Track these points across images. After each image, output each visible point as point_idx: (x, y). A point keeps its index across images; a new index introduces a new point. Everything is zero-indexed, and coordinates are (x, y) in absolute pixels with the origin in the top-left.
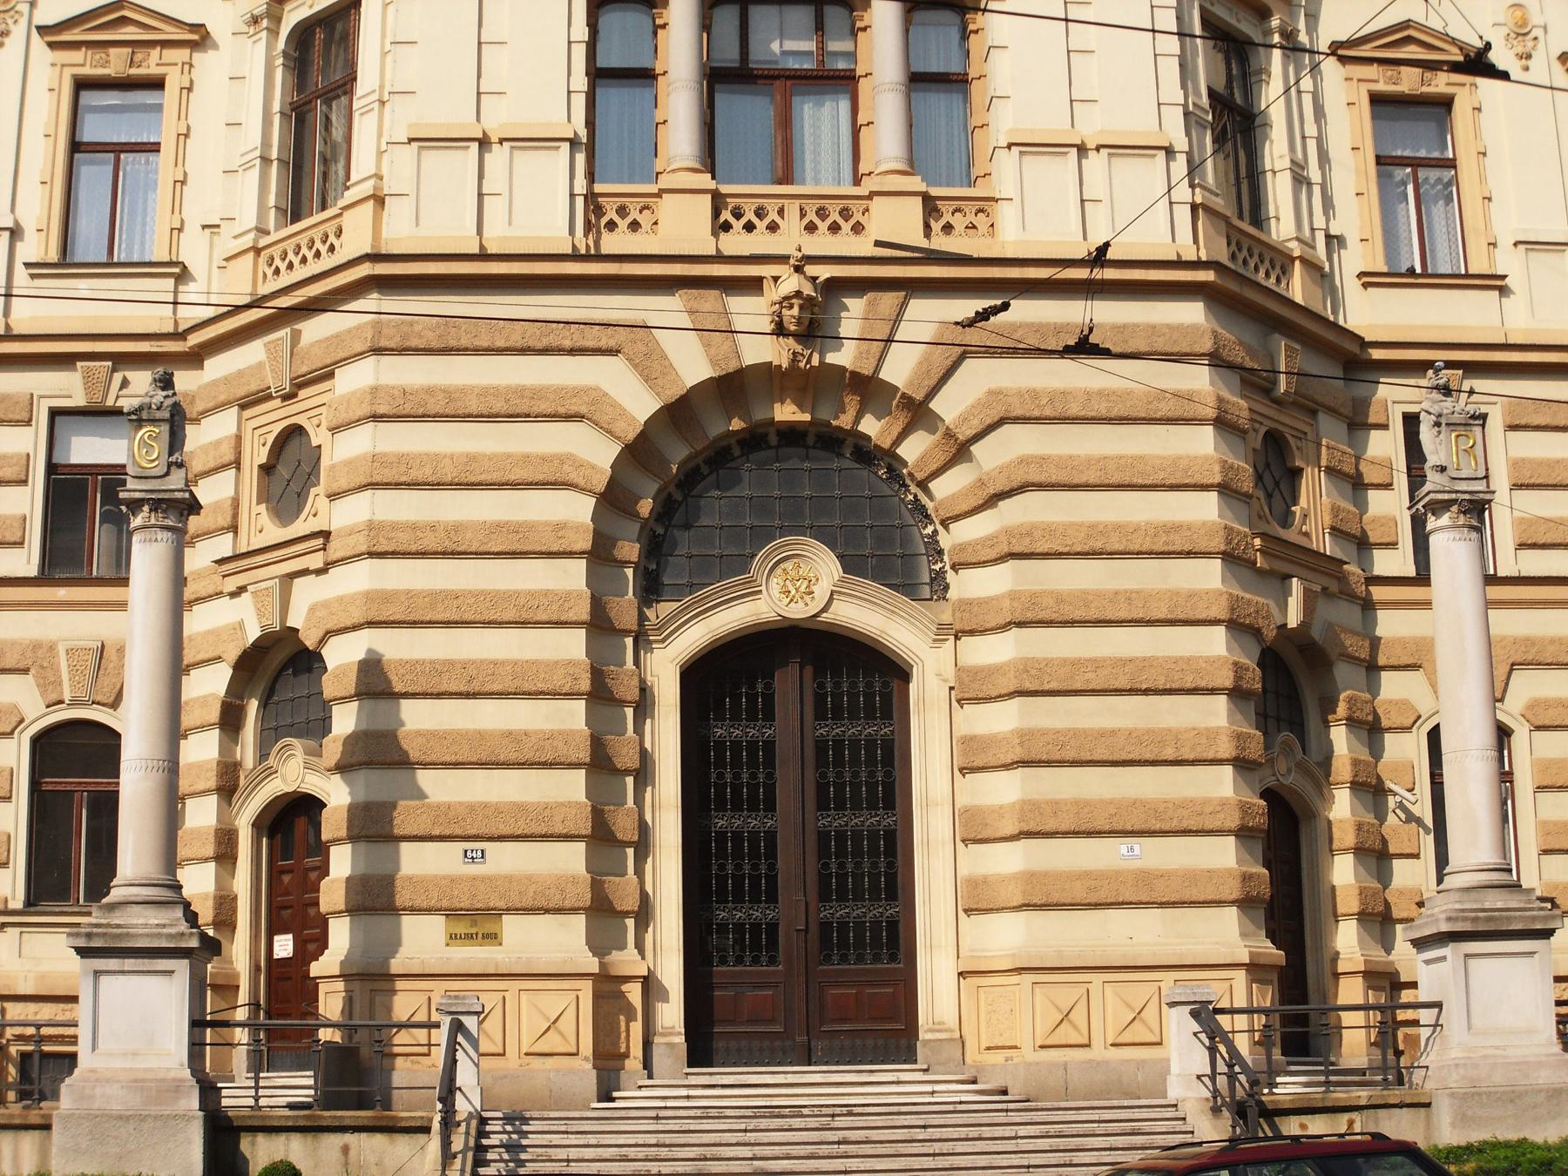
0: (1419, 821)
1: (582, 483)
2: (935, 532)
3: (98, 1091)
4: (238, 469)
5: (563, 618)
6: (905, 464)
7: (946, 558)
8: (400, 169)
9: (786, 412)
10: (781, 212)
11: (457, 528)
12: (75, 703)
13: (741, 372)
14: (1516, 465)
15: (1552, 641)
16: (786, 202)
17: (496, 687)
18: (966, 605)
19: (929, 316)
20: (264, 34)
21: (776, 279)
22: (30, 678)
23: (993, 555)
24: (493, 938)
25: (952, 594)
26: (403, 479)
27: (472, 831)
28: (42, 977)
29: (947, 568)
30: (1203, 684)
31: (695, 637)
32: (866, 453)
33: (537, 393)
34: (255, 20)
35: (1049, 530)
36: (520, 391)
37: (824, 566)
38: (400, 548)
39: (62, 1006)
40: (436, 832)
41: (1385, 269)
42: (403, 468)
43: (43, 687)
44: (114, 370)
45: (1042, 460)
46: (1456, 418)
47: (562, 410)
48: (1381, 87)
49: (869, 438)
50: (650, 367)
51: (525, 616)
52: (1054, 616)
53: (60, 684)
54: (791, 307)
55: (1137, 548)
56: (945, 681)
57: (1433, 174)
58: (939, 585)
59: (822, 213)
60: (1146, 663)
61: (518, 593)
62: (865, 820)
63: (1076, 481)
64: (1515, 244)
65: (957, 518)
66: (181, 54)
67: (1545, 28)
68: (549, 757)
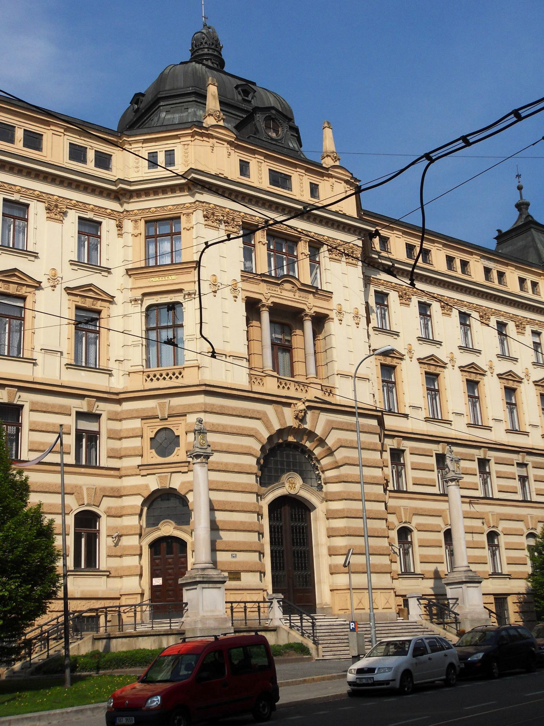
0: (396, 553)
1: (254, 454)
3: (208, 622)
4: (142, 438)
6: (314, 454)
9: (291, 439)
11: (227, 464)
12: (88, 505)
13: (314, 432)
14: (497, 472)
17: (238, 509)
18: (326, 493)
19: (324, 417)
22: (73, 496)
23: (337, 481)
24: (239, 579)
25: (324, 489)
27: (234, 549)
28: (82, 592)
31: (271, 497)
33: (243, 428)
34: (136, 300)
37: (299, 481)
39: (88, 601)
40: (226, 549)
41: (74, 363)
43: (78, 500)
44: (17, 392)
46: (457, 459)
48: (427, 370)
49: (307, 447)
50: (268, 425)
53: (84, 499)
57: (92, 335)
58: (320, 487)
61: (242, 483)
62: (302, 548)
64: (41, 350)
65: (326, 470)
66: (107, 304)
67: (62, 278)
68: (251, 529)
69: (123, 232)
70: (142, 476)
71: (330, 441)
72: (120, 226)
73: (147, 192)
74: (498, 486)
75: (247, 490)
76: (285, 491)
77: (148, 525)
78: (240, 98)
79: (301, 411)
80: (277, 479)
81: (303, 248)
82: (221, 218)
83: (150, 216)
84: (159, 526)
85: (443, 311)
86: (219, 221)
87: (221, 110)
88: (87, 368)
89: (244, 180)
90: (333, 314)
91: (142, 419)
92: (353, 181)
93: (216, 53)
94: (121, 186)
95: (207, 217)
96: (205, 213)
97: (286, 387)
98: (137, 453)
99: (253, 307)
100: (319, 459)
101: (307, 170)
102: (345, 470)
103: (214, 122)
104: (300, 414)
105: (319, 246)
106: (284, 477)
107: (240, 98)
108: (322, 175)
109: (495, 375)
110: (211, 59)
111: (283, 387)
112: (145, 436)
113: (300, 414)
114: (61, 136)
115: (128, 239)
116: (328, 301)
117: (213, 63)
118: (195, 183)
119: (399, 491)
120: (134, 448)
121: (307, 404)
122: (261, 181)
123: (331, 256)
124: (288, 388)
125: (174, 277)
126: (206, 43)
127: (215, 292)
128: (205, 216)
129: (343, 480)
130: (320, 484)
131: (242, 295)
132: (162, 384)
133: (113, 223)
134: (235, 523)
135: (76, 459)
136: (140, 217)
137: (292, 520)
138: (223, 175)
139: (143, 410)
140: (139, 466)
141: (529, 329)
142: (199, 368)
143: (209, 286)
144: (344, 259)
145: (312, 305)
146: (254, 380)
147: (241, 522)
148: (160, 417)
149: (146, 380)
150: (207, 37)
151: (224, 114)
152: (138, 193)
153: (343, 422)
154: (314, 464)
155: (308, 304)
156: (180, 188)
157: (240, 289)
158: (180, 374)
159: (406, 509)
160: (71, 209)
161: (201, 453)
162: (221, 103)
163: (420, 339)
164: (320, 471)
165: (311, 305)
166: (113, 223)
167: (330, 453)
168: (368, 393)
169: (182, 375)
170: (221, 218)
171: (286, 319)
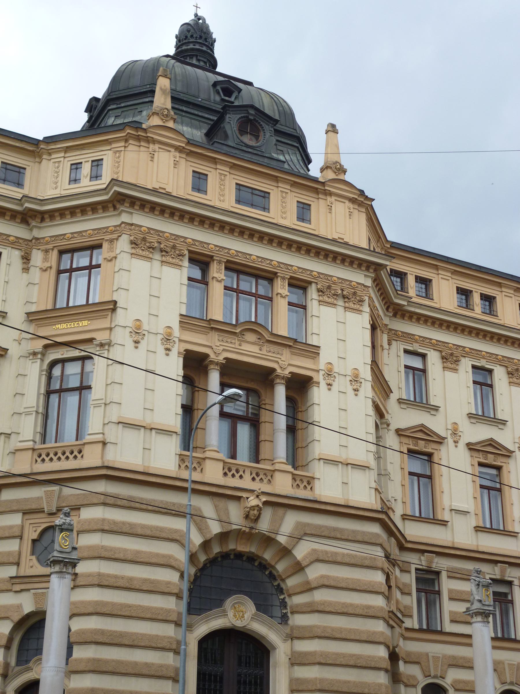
2: (285, 598)
4: (21, 539)
5: (168, 619)
7: (288, 608)
8: (113, 434)
10: (244, 472)
11: (131, 579)
12: (512, 683)
14: (450, 591)
15: (461, 658)
16: (246, 468)
17: (142, 644)
18: (292, 629)
20: (39, 361)
21: (248, 498)
23: (309, 609)
25: (290, 622)
26: (113, 557)
29: (289, 612)
30: (377, 666)
31: (203, 629)
32: (264, 566)
33: (162, 529)
34: (35, 354)
35: (330, 603)
36: (157, 528)
37: (249, 608)
38: (110, 584)
42: (113, 553)
45: (327, 577)
47: (170, 537)
48: (412, 447)
51: (154, 617)
52: (331, 636)
54: (254, 510)
55: (357, 613)
56: (287, 656)
58: (284, 619)
59: (258, 475)
60: (358, 657)
63: (339, 586)
65: (295, 594)
68: (160, 674)
69: (30, 264)
70: (16, 592)
71: (301, 552)
72: (26, 259)
73: (62, 213)
74: (450, 612)
75: (160, 617)
76: (228, 621)
77: (19, 662)
78: (218, 98)
79: (253, 508)
80: (219, 603)
81: (281, 287)
82: (156, 245)
83: (64, 244)
84: (31, 664)
85: (511, 380)
86: (153, 249)
87: (173, 108)
88: (491, 531)
89: (197, 197)
90: (319, 378)
91: (24, 514)
92: (362, 200)
93: (204, 48)
94: (27, 205)
95: (135, 243)
96: (132, 238)
97: (237, 476)
98: (11, 560)
99: (195, 366)
100: (283, 577)
101: (294, 184)
102: (320, 596)
103: (160, 123)
104: (252, 512)
105: (306, 285)
106: (229, 603)
107: (218, 98)
108: (316, 191)
109: (462, 445)
110: (197, 56)
111: (305, 487)
112: (25, 536)
113: (252, 512)
114: (511, 297)
115: (35, 274)
116: (313, 358)
117: (199, 60)
118: (121, 199)
119: (429, 631)
120: (10, 553)
121: (264, 499)
122: (222, 198)
123: (321, 298)
124: (241, 477)
125: (85, 323)
126: (192, 36)
127: (137, 342)
128: (132, 242)
129: (316, 609)
130: (286, 614)
131: (177, 349)
132: (56, 465)
133: (17, 254)
134: (136, 664)
135: (494, 632)
136: (50, 246)
137: (240, 664)
138: (165, 189)
139: (26, 500)
140: (11, 578)
141: (466, 364)
142: (104, 443)
143: (129, 334)
144: (340, 302)
145: (287, 364)
146: (298, 482)
147: (146, 664)
148: (46, 510)
149: (36, 461)
150: (194, 30)
151: (175, 113)
152: (52, 215)
153: (323, 526)
154: (279, 585)
155: (280, 362)
156: (104, 206)
157: (176, 340)
158: (80, 452)
159: (436, 658)
160: (465, 357)
161: (61, 559)
162: (174, 99)
163: (470, 416)
164: (286, 595)
165: (287, 363)
166: (17, 254)
167: (299, 568)
168: (367, 488)
169: (81, 454)
170: (156, 245)
171: (253, 380)
